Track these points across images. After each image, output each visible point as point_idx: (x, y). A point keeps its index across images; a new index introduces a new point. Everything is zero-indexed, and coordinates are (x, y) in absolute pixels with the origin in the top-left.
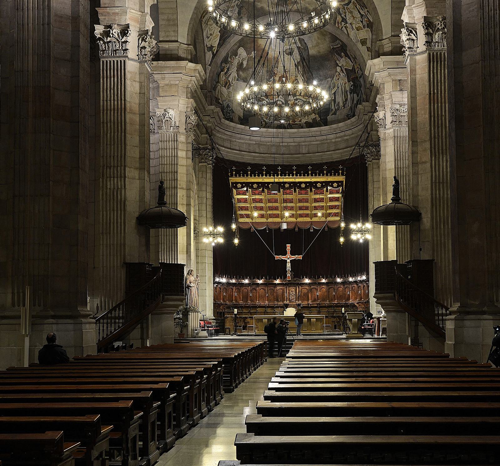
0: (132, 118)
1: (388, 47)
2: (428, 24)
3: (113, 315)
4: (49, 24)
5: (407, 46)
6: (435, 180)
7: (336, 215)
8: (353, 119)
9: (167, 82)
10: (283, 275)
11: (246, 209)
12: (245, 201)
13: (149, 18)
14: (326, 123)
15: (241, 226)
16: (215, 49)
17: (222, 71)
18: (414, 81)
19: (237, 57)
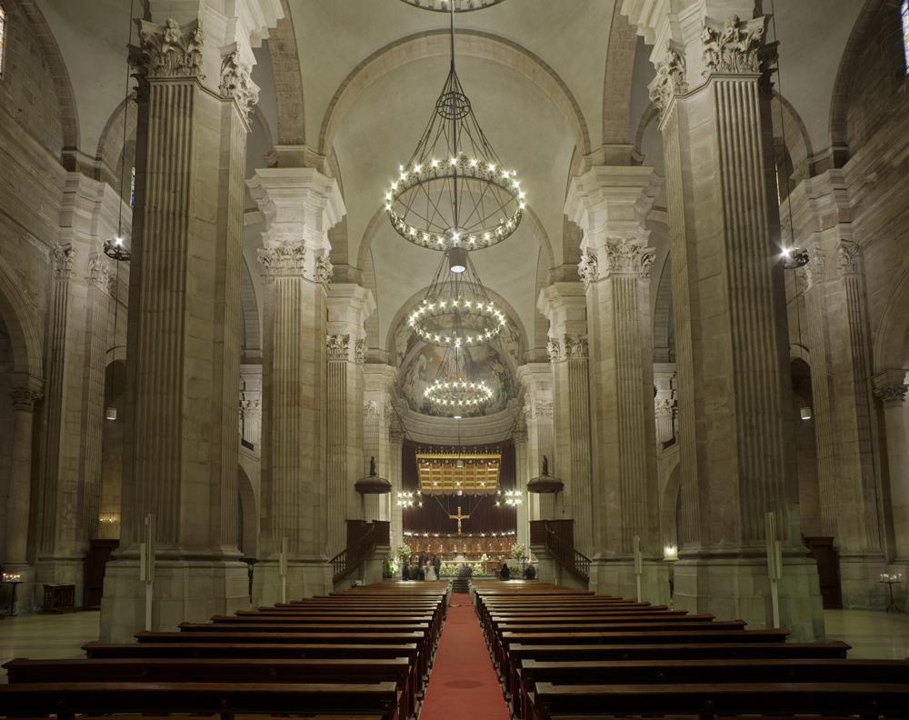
0: (352, 408)
2: (568, 340)
7: (494, 484)
8: (504, 411)
11: (428, 479)
12: (427, 473)
14: (484, 414)
18: (557, 383)
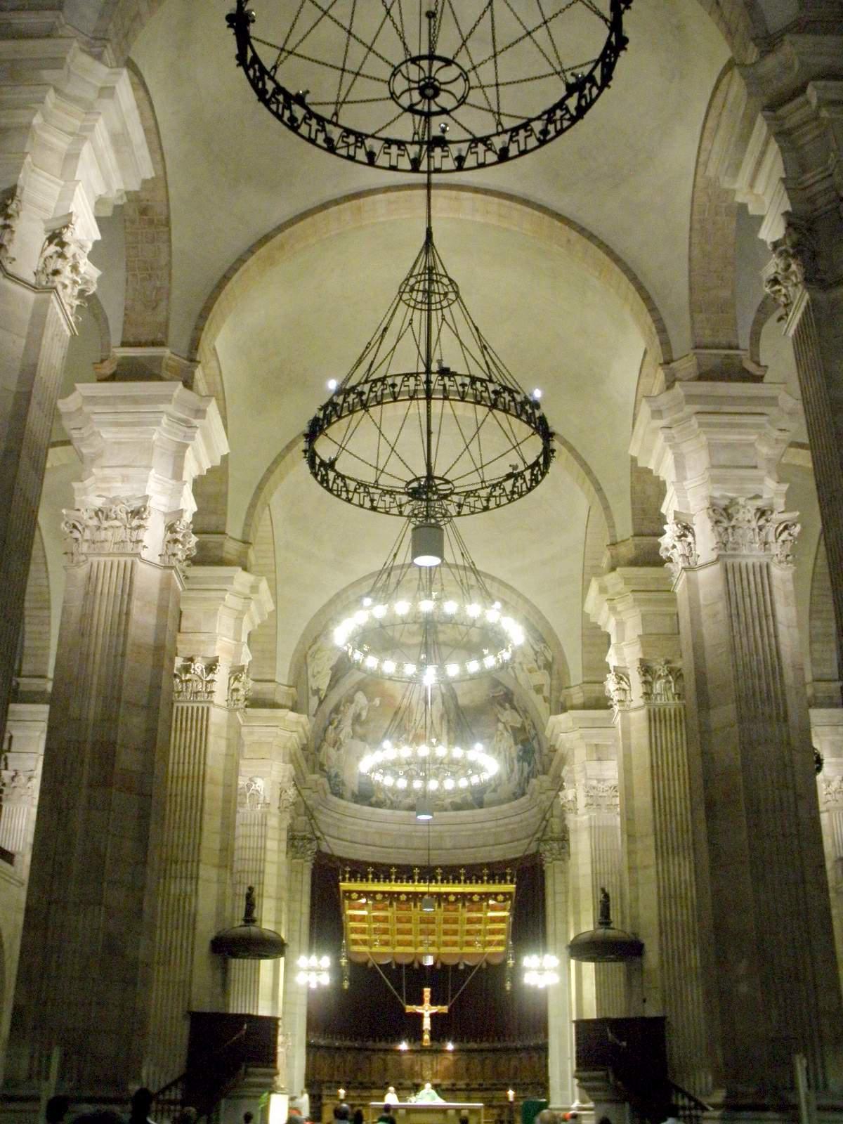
1: (578, 698)
2: (646, 669)
3: (167, 1097)
4: (123, 655)
5: (616, 698)
7: (499, 943)
8: (523, 800)
9: (255, 738)
10: (416, 1034)
12: (362, 919)
13: (245, 649)
15: (353, 958)
16: (323, 694)
17: (331, 724)
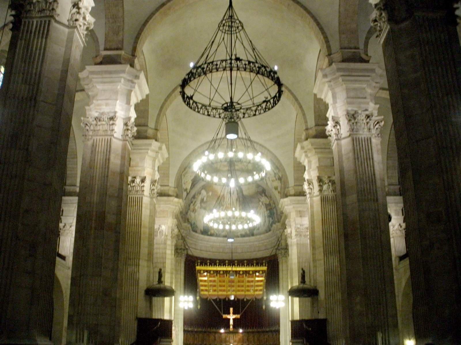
0: (145, 231)
1: (292, 192)
2: (320, 180)
4: (107, 177)
6: (327, 271)
8: (270, 233)
10: (227, 326)
13: (157, 173)
17: (192, 202)
19: (201, 195)
